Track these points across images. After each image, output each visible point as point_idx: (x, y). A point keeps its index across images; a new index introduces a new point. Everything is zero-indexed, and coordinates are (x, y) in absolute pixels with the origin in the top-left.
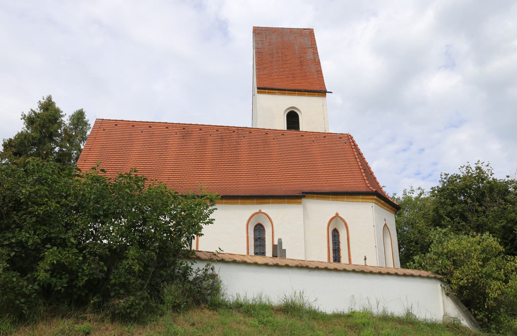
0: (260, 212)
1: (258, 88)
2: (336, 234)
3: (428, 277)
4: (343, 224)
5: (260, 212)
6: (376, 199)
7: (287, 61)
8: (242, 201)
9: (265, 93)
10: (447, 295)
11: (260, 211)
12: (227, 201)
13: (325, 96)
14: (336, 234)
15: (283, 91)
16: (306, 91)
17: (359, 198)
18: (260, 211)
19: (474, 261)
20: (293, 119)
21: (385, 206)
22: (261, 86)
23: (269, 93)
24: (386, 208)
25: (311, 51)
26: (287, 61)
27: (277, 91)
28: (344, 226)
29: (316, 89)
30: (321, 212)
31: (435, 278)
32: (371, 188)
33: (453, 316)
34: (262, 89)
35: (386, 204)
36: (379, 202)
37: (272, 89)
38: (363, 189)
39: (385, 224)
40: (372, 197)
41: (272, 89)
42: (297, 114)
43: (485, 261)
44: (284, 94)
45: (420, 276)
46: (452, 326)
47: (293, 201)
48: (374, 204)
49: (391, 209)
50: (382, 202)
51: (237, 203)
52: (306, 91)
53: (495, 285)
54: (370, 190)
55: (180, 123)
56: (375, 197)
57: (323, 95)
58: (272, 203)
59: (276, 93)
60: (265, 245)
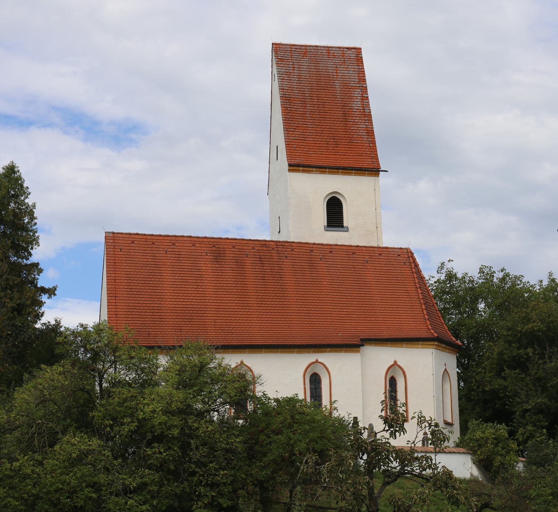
0: (317, 361)
1: (290, 165)
2: (392, 383)
3: (464, 453)
4: (401, 372)
5: (317, 361)
6: (436, 345)
7: (325, 110)
8: (299, 350)
9: (298, 171)
10: (474, 463)
11: (317, 360)
12: (282, 350)
13: (378, 175)
14: (392, 383)
15: (322, 169)
16: (353, 169)
17: (419, 344)
18: (317, 360)
19: (489, 445)
20: (335, 211)
21: (446, 348)
22: (293, 162)
23: (303, 171)
24: (447, 351)
25: (357, 93)
26: (325, 110)
27: (314, 169)
28: (402, 375)
29: (365, 165)
30: (380, 358)
31: (468, 453)
32: (432, 331)
33: (467, 476)
34: (294, 167)
35: (447, 347)
36: (440, 346)
37: (309, 166)
38: (424, 335)
39: (446, 370)
40: (433, 343)
41: (309, 166)
42: (340, 201)
43: (496, 445)
44: (324, 173)
45: (459, 453)
46: (473, 481)
47: (351, 349)
48: (434, 351)
49: (452, 350)
50: (443, 346)
51: (293, 352)
52: (353, 169)
53: (499, 458)
54: (433, 337)
55: (208, 236)
56: (436, 343)
57: (376, 174)
58: (330, 352)
59: (313, 171)
60: (321, 396)
